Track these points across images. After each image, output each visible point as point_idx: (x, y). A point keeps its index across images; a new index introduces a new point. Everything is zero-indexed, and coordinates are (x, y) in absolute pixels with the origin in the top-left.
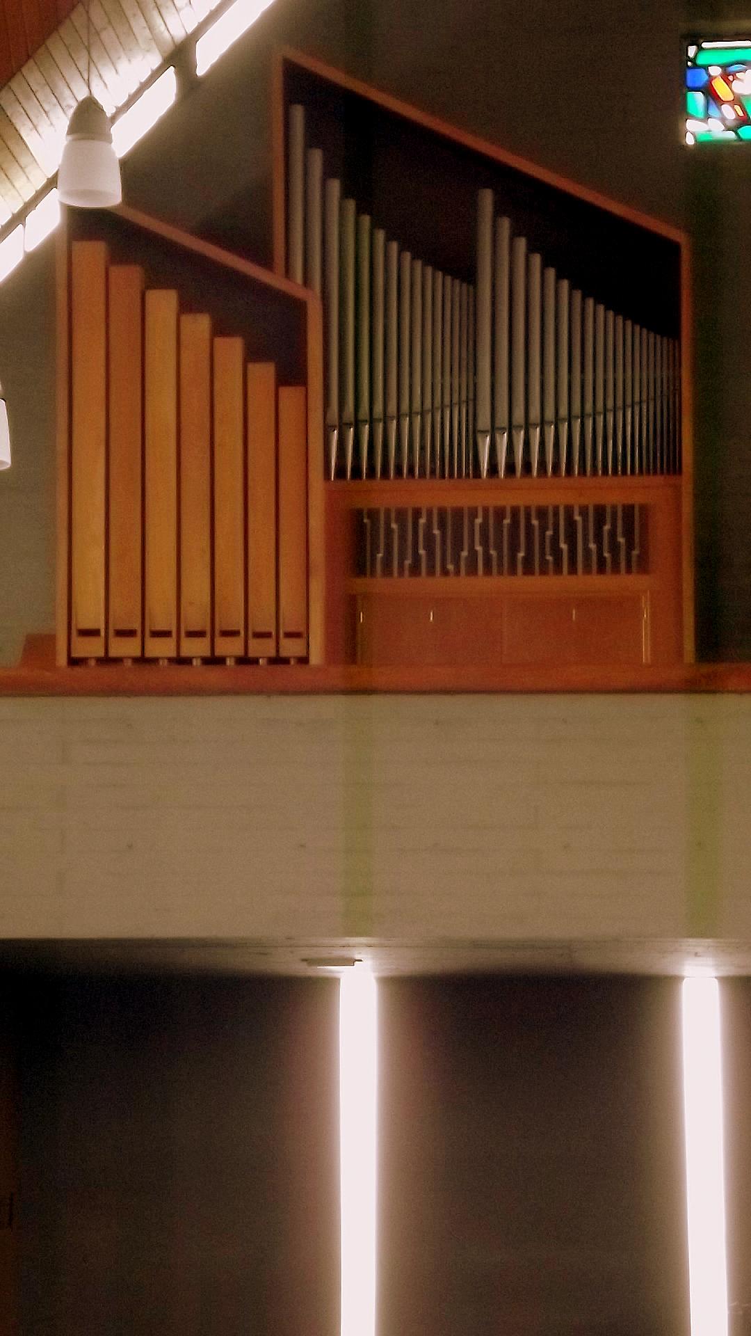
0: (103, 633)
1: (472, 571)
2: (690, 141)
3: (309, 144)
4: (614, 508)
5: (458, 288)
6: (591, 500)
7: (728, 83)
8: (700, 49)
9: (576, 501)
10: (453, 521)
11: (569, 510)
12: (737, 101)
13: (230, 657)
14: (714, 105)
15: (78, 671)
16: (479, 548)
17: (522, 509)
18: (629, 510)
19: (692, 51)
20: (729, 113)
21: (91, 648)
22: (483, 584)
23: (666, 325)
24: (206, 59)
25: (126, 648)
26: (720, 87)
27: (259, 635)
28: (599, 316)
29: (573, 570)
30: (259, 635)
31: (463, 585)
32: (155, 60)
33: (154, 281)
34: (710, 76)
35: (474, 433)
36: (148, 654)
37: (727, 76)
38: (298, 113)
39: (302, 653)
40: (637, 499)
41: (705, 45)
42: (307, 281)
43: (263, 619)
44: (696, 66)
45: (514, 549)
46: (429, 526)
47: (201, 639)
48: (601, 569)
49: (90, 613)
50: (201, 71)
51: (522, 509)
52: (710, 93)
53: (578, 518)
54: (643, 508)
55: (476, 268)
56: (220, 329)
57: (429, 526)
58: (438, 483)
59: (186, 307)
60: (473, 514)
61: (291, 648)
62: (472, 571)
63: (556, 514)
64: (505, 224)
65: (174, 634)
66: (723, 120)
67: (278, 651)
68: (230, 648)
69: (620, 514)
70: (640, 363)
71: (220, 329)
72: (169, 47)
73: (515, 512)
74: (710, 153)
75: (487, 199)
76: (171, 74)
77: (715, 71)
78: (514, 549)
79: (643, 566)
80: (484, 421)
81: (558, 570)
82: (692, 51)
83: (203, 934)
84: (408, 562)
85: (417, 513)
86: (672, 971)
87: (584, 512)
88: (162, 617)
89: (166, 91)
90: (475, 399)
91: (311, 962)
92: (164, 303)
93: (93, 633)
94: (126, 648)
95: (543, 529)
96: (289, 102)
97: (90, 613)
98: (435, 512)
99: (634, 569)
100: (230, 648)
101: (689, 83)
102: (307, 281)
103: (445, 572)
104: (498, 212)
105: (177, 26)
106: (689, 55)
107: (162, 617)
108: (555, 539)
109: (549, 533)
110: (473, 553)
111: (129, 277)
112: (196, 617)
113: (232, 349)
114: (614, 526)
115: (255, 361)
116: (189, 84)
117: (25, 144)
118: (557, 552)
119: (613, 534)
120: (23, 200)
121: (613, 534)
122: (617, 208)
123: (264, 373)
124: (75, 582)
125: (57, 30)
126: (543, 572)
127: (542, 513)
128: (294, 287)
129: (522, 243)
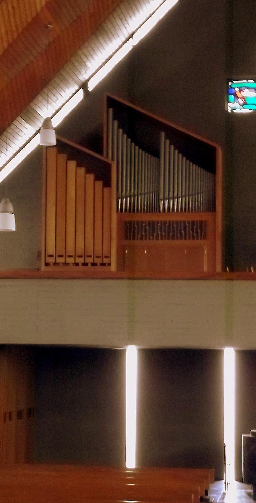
1: (157, 239)
3: (114, 119)
4: (197, 221)
6: (191, 219)
7: (240, 92)
8: (232, 82)
9: (187, 220)
10: (152, 225)
11: (185, 222)
12: (243, 98)
13: (90, 263)
16: (159, 232)
17: (155, 239)
18: (201, 222)
19: (230, 83)
21: (51, 260)
22: (160, 242)
23: (107, 184)
24: (91, 87)
25: (61, 260)
26: (238, 94)
27: (97, 257)
28: (194, 167)
30: (97, 257)
31: (154, 242)
32: (77, 87)
33: (70, 158)
34: (235, 91)
35: (158, 200)
36: (67, 262)
38: (111, 110)
39: (109, 262)
40: (203, 219)
41: (234, 82)
43: (99, 252)
44: (231, 87)
45: (169, 232)
46: (145, 226)
48: (193, 239)
49: (51, 250)
50: (90, 89)
51: (155, 239)
53: (187, 224)
54: (205, 222)
56: (88, 171)
57: (145, 226)
58: (149, 214)
59: (79, 165)
60: (158, 222)
61: (106, 261)
62: (157, 239)
64: (168, 142)
65: (74, 257)
66: (239, 103)
67: (102, 262)
68: (89, 260)
69: (199, 223)
71: (88, 171)
72: (80, 84)
73: (169, 222)
74: (233, 116)
75: (163, 134)
76: (81, 91)
77: (237, 89)
78: (169, 232)
79: (205, 238)
80: (161, 197)
81: (181, 238)
82: (230, 83)
84: (139, 236)
85: (142, 222)
87: (189, 223)
88: (71, 251)
89: (80, 96)
90: (159, 190)
92: (72, 164)
93: (52, 256)
94: (61, 260)
95: (177, 227)
96: (108, 107)
97: (51, 250)
98: (147, 222)
99: (202, 238)
100: (89, 260)
101: (230, 92)
102: (107, 157)
103: (150, 239)
105: (84, 76)
106: (229, 84)
107: (71, 251)
108: (181, 230)
109: (179, 228)
110: (158, 234)
111: (63, 157)
113: (91, 177)
115: (97, 180)
116: (86, 92)
117: (38, 113)
118: (181, 233)
119: (197, 229)
120: (122, 40)
122: (198, 137)
123: (100, 184)
124: (47, 241)
126: (177, 239)
127: (177, 223)
128: (109, 160)
129: (172, 147)
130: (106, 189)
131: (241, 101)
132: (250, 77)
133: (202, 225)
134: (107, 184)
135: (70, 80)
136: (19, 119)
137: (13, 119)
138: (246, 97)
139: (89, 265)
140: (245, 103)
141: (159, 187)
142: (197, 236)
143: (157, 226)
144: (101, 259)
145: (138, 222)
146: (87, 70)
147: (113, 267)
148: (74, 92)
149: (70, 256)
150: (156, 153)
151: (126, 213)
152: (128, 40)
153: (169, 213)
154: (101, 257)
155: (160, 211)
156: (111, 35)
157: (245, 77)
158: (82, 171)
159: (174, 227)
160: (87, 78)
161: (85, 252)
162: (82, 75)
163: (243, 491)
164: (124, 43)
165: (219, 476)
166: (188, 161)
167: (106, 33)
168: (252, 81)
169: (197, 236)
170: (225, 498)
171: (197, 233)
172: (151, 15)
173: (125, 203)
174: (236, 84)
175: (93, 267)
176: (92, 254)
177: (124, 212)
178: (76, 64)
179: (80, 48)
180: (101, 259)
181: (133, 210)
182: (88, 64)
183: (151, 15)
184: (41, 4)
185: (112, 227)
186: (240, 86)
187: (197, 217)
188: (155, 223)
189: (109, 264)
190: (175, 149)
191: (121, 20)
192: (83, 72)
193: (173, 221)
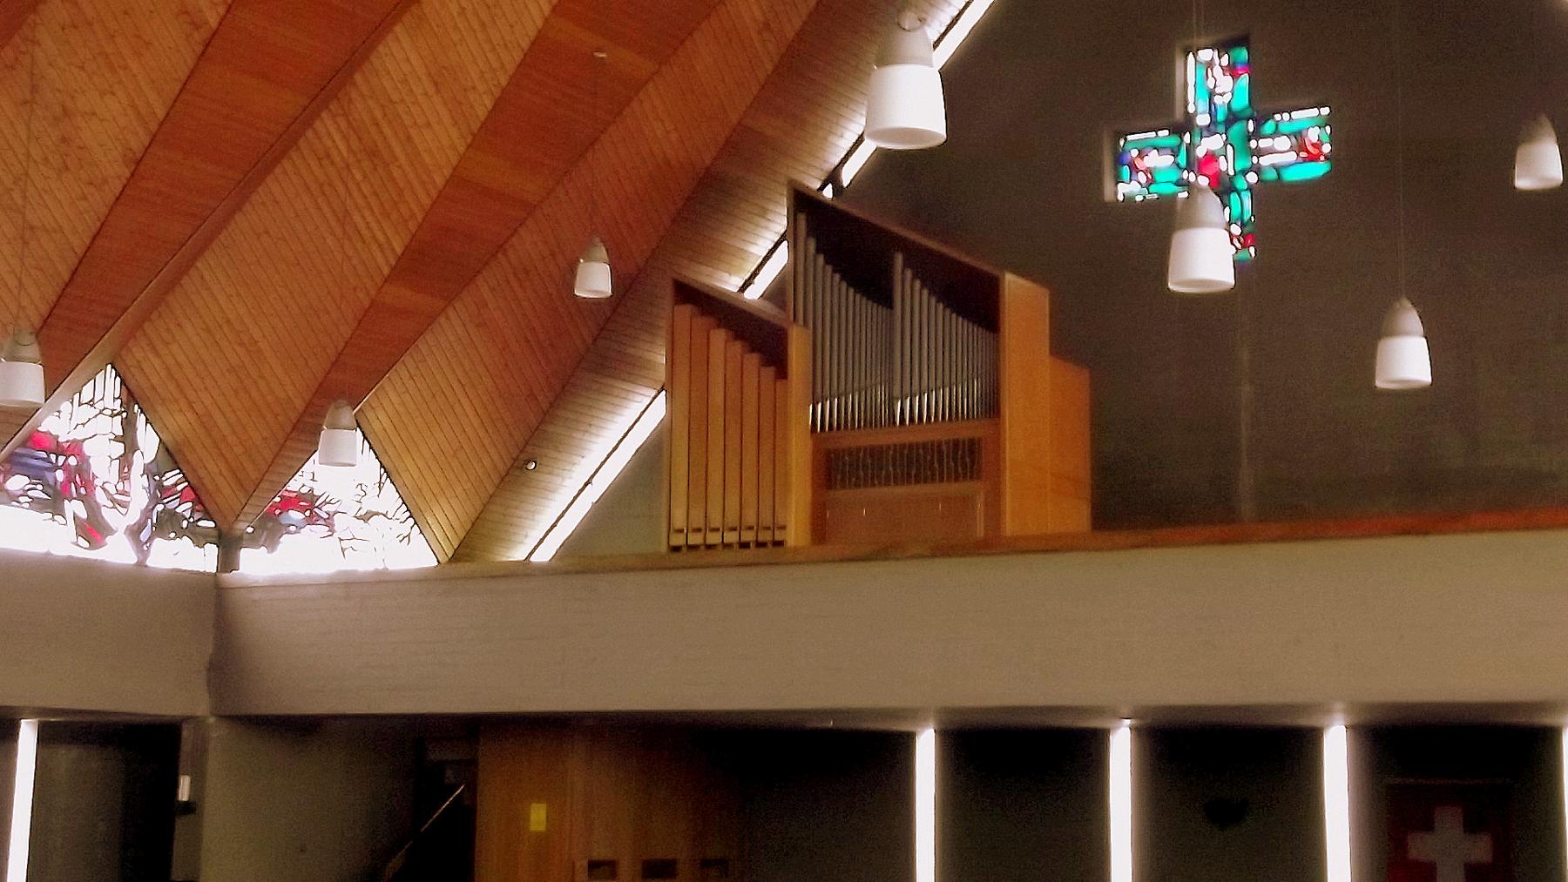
0: (685, 531)
3: (808, 234)
5: (883, 311)
8: (1126, 139)
10: (876, 453)
12: (1148, 171)
15: (675, 556)
18: (972, 441)
21: (678, 540)
24: (847, 176)
26: (1139, 163)
29: (942, 480)
37: (1141, 155)
41: (1130, 138)
43: (750, 519)
47: (698, 534)
50: (845, 184)
52: (1134, 169)
55: (998, 287)
60: (889, 447)
63: (964, 444)
70: (911, 359)
75: (899, 259)
80: (897, 392)
81: (933, 480)
82: (1122, 142)
83: (1076, 703)
85: (859, 450)
88: (716, 521)
104: (905, 266)
107: (716, 521)
109: (929, 458)
112: (732, 519)
113: (753, 360)
114: (964, 452)
121: (963, 458)
122: (966, 259)
127: (924, 446)
130: (778, 384)
131: (1142, 177)
132: (1157, 123)
134: (782, 373)
138: (1155, 168)
141: (891, 371)
142: (933, 475)
144: (770, 532)
145: (850, 452)
151: (930, 426)
153: (903, 427)
154: (755, 528)
155: (894, 423)
157: (1152, 123)
158: (737, 347)
159: (918, 454)
160: (836, 161)
161: (740, 522)
166: (948, 311)
168: (1166, 132)
171: (964, 466)
173: (828, 409)
175: (710, 552)
180: (770, 532)
181: (843, 425)
184: (541, 10)
186: (1140, 145)
187: (965, 432)
188: (860, 449)
190: (922, 287)
193: (917, 444)
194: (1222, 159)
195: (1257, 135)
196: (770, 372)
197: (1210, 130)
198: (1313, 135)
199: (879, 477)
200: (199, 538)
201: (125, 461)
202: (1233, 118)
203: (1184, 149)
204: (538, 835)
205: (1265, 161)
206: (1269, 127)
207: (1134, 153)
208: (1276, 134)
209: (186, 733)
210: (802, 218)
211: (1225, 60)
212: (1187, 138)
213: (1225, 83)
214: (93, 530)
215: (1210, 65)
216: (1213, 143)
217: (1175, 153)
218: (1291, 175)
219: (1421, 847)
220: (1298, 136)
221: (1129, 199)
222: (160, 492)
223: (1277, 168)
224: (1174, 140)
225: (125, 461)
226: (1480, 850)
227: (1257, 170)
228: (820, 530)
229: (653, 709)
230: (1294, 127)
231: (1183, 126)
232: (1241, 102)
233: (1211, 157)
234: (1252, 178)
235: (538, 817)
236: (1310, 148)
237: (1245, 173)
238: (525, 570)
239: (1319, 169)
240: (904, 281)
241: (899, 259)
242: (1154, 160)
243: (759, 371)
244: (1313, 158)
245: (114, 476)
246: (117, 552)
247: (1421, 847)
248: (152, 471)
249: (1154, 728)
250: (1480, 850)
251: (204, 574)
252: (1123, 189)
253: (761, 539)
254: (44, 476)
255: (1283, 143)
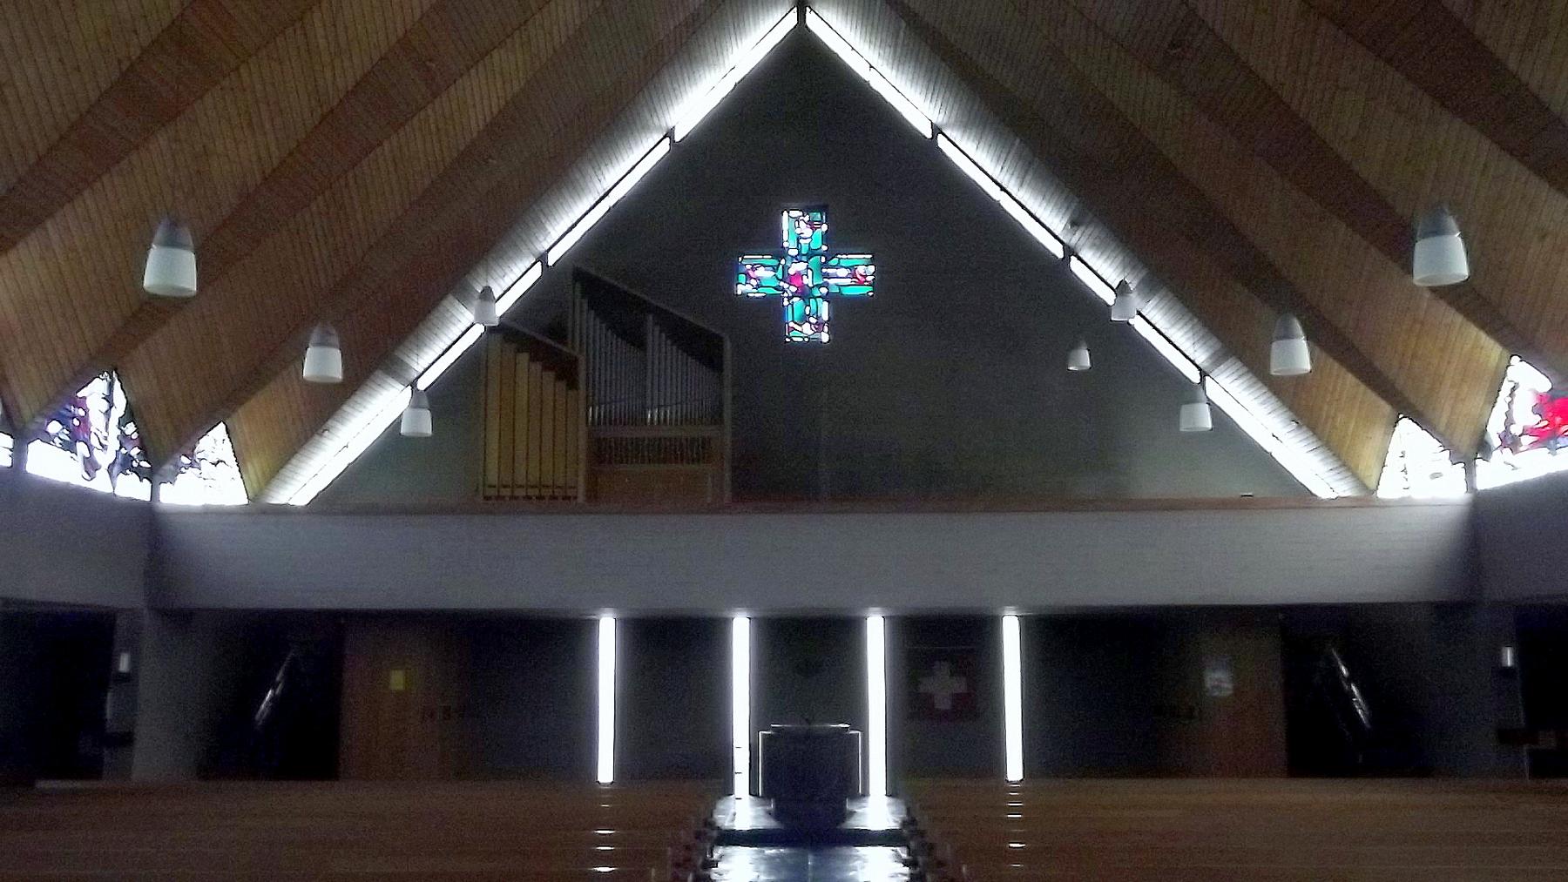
2: (739, 293)
14: (1119, 262)
20: (754, 282)
21: (492, 492)
23: (572, 384)
24: (552, 258)
26: (751, 273)
37: (753, 269)
41: (745, 257)
42: (581, 351)
43: (560, 482)
49: (493, 478)
56: (545, 368)
59: (532, 359)
61: (570, 493)
68: (547, 492)
71: (545, 368)
75: (650, 317)
80: (649, 402)
82: (740, 259)
86: (730, 616)
89: (537, 272)
91: (581, 615)
92: (524, 358)
100: (547, 492)
102: (573, 348)
107: (521, 480)
113: (549, 376)
116: (545, 266)
125: (6, 252)
128: (575, 354)
132: (767, 251)
133: (706, 442)
134: (572, 384)
135: (525, 251)
136: (450, 297)
137: (443, 297)
139: (547, 499)
140: (758, 286)
143: (1361, 402)
146: (547, 235)
147: (581, 499)
148: (528, 266)
149: (521, 486)
150: (639, 343)
152: (602, 198)
155: (646, 424)
156: (581, 194)
162: (541, 242)
163: (760, 808)
164: (597, 203)
165: (727, 790)
167: (574, 188)
169: (676, 458)
170: (736, 820)
172: (634, 167)
174: (747, 262)
176: (551, 483)
177: (592, 626)
178: (531, 224)
179: (536, 201)
182: (550, 229)
183: (634, 167)
185: (1291, 510)
189: (576, 498)
191: (593, 168)
192: (541, 238)
194: (805, 277)
195: (826, 265)
196: (562, 385)
197: (797, 259)
198: (861, 270)
199: (637, 457)
200: (140, 473)
201: (107, 413)
202: (812, 253)
203: (781, 266)
204: (399, 693)
205: (832, 281)
206: (834, 262)
207: (749, 267)
208: (837, 267)
209: (121, 622)
210: (578, 285)
211: (807, 219)
212: (783, 262)
213: (808, 232)
214: (90, 466)
215: (797, 219)
216: (796, 268)
217: (775, 269)
218: (847, 292)
219: (928, 685)
220: (852, 268)
221: (745, 295)
222: (124, 439)
223: (839, 286)
224: (774, 262)
225: (107, 413)
226: (959, 686)
227: (826, 285)
228: (593, 494)
229: (483, 606)
230: (850, 263)
231: (780, 253)
232: (817, 243)
233: (799, 275)
234: (824, 291)
235: (397, 680)
236: (859, 276)
237: (819, 286)
238: (285, 511)
239: (865, 290)
240: (654, 334)
241: (650, 317)
242: (761, 272)
243: (554, 385)
244: (861, 284)
245: (103, 428)
246: (101, 484)
247: (928, 685)
248: (122, 423)
249: (769, 619)
250: (959, 686)
251: (145, 501)
252: (740, 289)
253: (487, 494)
254: (68, 422)
255: (843, 272)
